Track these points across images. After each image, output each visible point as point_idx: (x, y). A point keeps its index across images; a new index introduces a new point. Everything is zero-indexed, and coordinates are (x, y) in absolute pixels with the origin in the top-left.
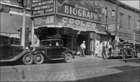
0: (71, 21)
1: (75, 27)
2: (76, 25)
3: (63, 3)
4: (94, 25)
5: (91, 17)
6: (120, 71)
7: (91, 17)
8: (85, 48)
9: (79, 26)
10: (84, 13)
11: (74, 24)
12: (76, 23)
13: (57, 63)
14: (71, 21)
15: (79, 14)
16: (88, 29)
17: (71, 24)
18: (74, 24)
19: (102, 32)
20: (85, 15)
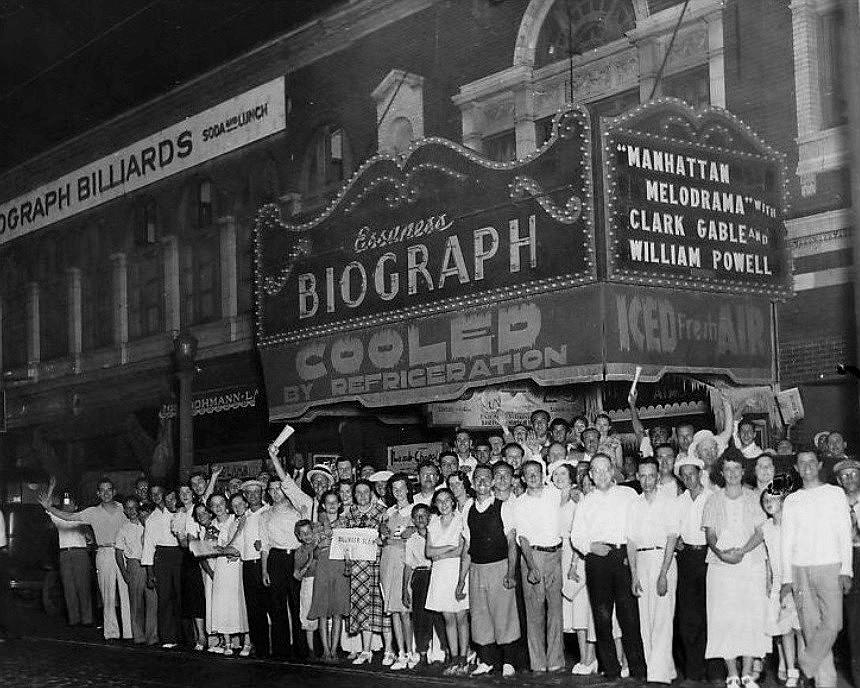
0: (345, 355)
1: (377, 388)
2: (383, 370)
3: (758, 238)
4: (522, 326)
5: (479, 267)
6: (311, 646)
7: (479, 267)
8: (852, 575)
9: (398, 368)
10: (723, 228)
11: (367, 367)
12: (377, 359)
13: (519, 612)
14: (345, 355)
15: (380, 288)
16: (474, 372)
17: (347, 376)
18: (367, 367)
19: (611, 366)
20: (426, 273)
